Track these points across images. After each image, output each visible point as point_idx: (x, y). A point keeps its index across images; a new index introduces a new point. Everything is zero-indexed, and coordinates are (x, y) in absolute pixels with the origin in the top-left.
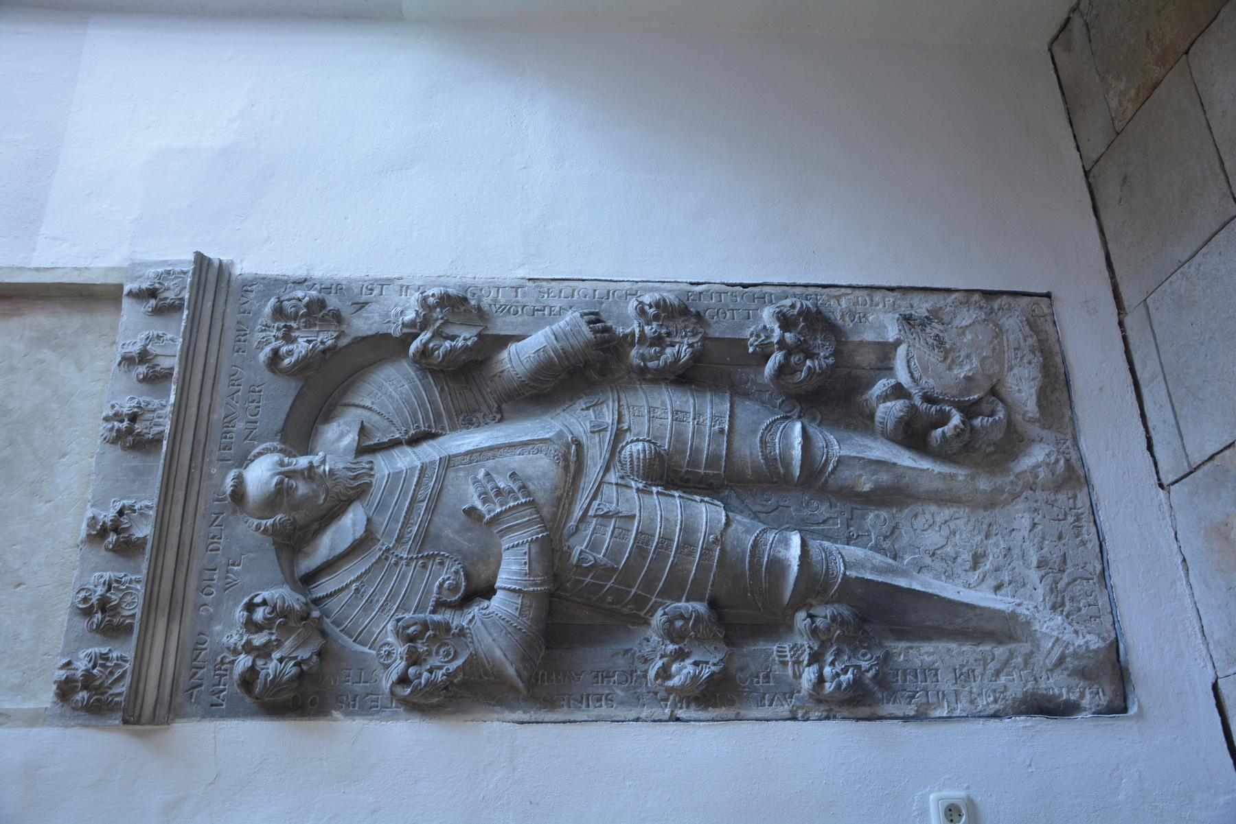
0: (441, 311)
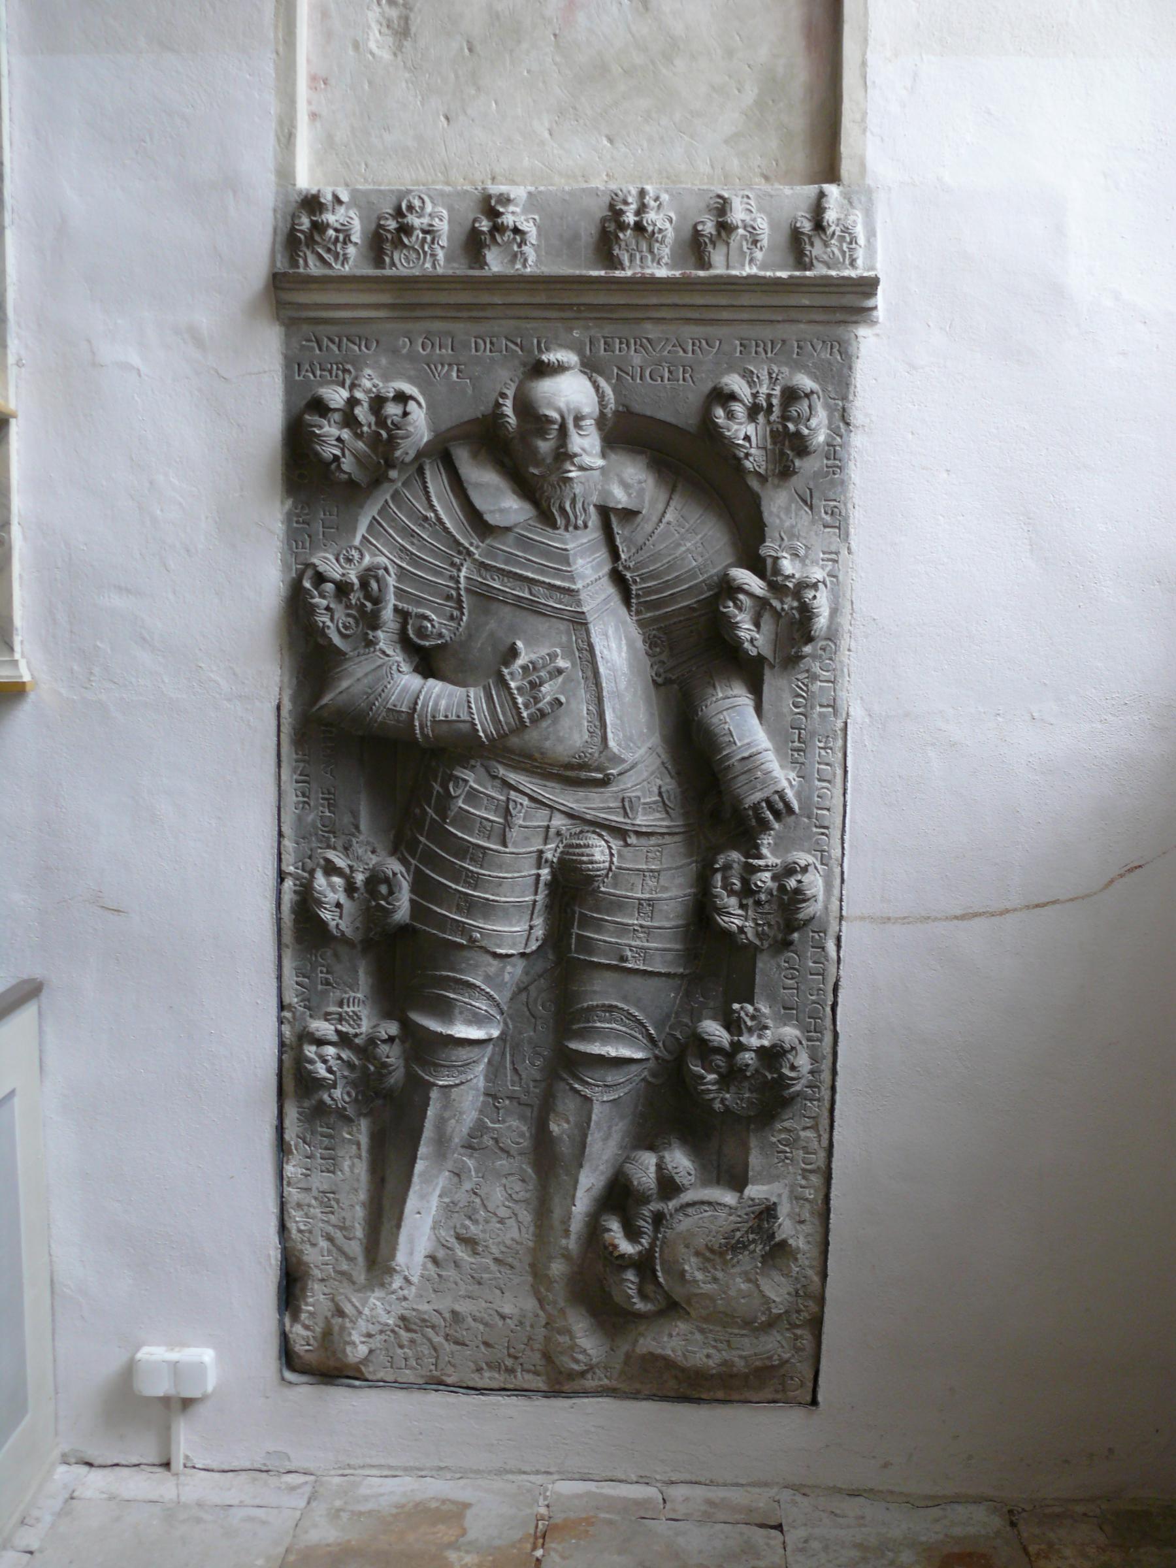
0: (792, 608)
